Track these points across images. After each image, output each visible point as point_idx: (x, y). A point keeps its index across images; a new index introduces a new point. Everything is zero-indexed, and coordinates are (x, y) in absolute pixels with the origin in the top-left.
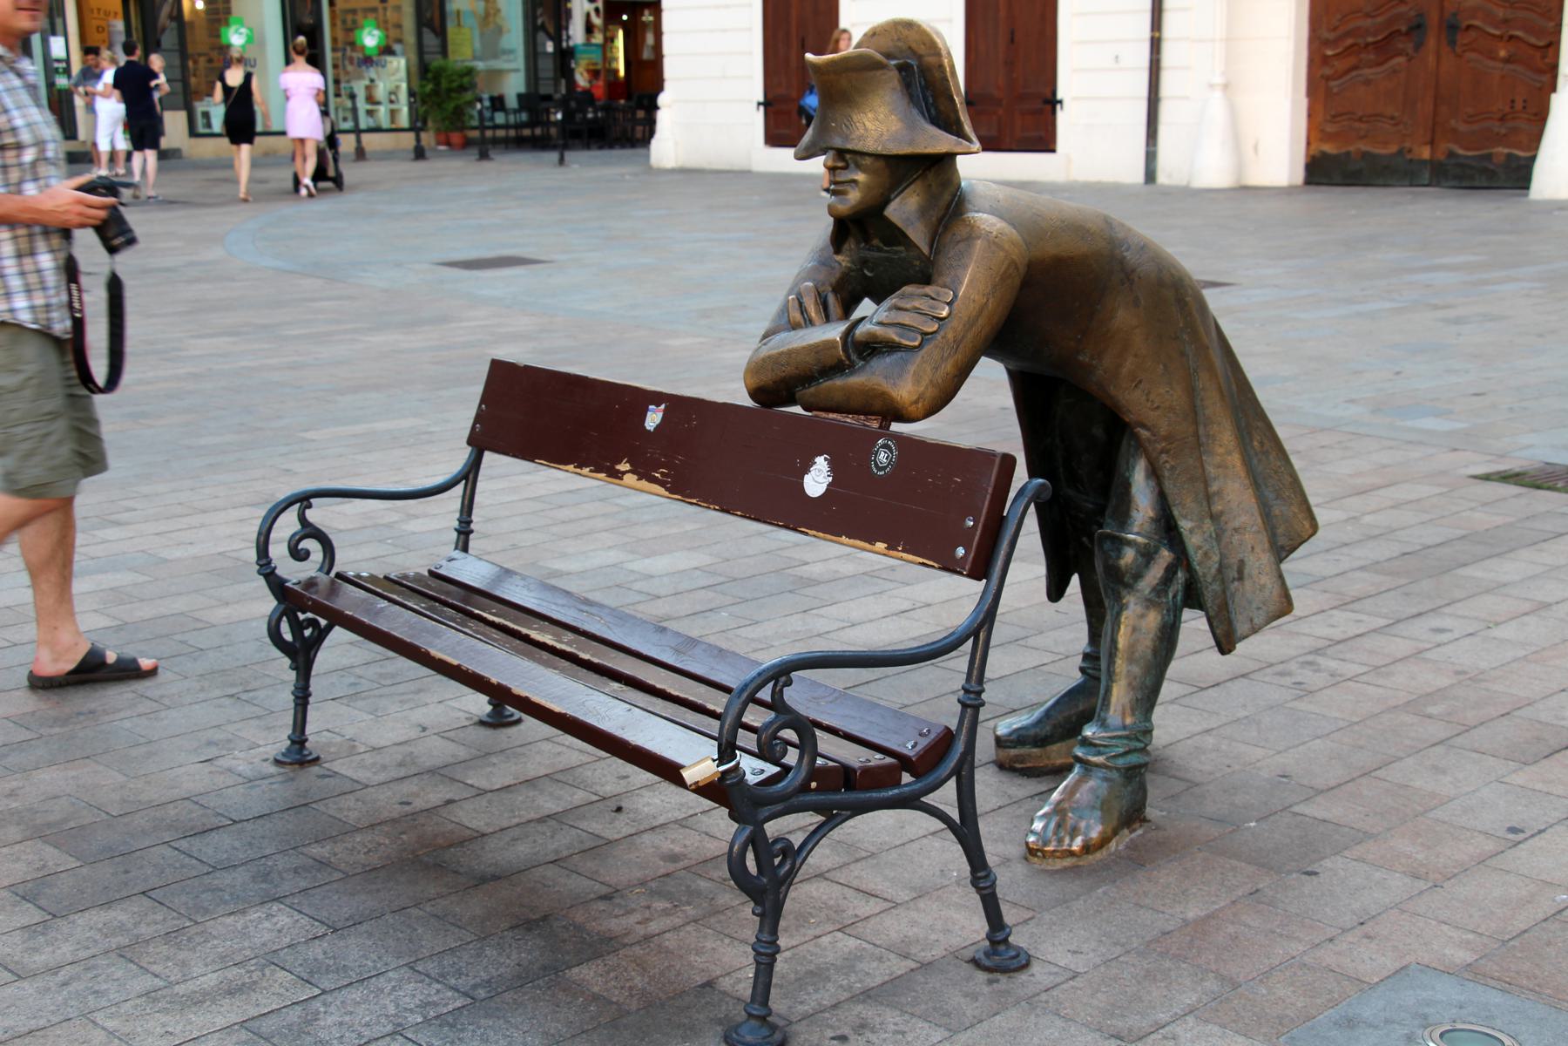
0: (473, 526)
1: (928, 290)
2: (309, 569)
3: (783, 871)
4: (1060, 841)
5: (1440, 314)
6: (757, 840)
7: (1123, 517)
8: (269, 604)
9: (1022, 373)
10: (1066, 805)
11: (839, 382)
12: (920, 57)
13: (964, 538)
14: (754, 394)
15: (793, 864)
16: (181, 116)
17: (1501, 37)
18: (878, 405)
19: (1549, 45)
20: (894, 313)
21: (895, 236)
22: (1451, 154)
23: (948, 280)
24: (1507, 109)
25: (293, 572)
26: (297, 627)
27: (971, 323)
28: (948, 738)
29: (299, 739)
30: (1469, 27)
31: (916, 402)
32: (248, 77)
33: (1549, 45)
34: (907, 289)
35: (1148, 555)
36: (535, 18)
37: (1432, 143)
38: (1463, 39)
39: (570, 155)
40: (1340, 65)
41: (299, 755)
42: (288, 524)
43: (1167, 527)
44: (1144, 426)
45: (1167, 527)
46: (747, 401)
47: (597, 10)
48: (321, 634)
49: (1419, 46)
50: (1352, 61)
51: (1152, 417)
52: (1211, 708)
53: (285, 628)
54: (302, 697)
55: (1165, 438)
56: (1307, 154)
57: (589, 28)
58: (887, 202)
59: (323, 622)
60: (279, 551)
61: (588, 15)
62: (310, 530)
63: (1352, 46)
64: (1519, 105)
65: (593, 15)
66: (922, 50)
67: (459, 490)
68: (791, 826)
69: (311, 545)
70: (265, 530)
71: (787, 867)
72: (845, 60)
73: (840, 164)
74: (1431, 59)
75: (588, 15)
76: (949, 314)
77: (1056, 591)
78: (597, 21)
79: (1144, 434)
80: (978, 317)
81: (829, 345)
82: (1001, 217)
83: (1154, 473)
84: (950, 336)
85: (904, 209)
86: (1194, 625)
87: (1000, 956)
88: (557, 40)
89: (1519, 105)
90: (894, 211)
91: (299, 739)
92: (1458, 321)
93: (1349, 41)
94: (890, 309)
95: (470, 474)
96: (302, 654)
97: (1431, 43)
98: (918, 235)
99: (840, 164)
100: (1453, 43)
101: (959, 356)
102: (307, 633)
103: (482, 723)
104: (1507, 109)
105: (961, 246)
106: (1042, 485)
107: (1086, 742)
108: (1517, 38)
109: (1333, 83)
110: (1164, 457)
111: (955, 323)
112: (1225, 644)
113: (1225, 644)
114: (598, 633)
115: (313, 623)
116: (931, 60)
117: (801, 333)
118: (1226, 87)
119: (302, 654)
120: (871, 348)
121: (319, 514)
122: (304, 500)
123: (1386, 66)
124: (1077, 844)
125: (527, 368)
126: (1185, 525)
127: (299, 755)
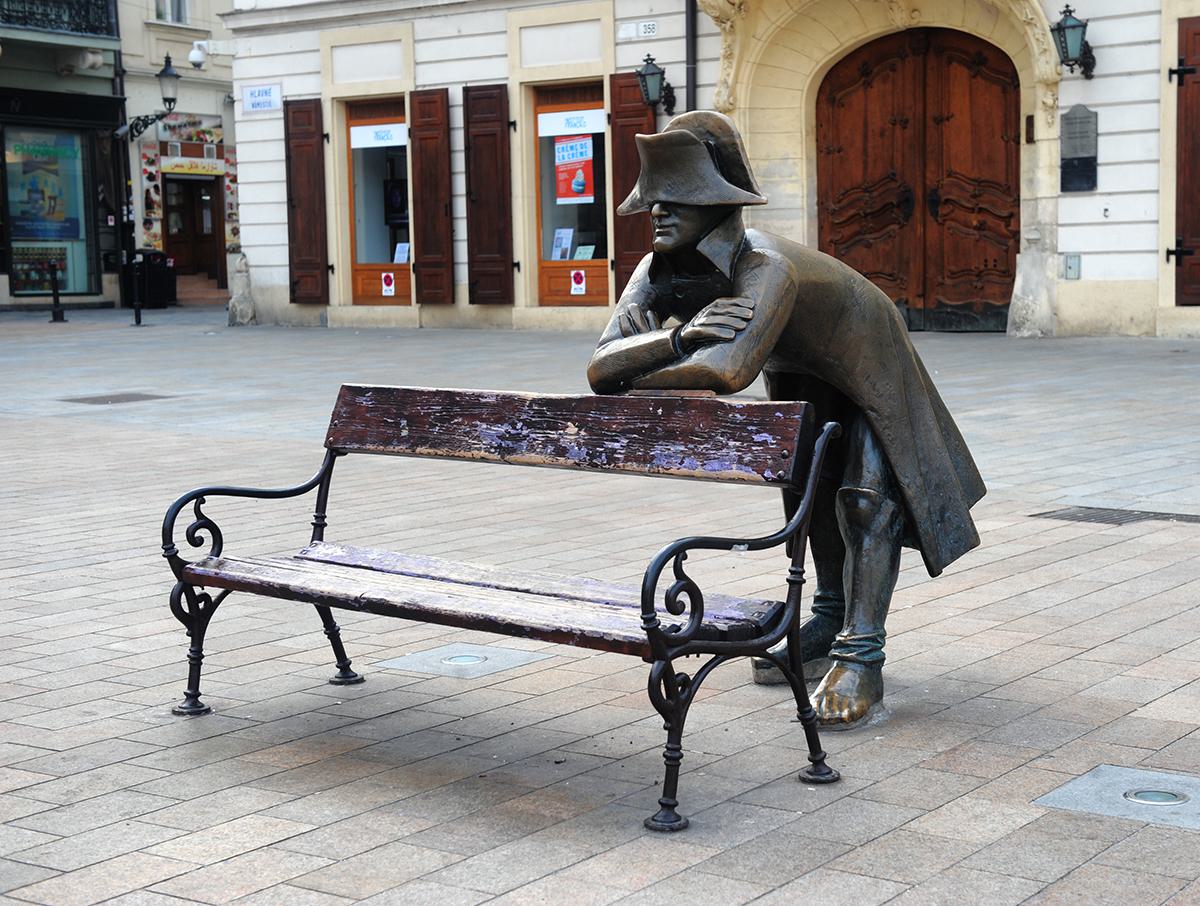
0: (326, 520)
1: (734, 301)
3: (683, 697)
4: (832, 711)
6: (666, 673)
7: (857, 476)
8: (172, 580)
10: (832, 689)
12: (717, 138)
14: (595, 386)
15: (690, 691)
17: (973, 209)
19: (1011, 215)
20: (712, 317)
21: (706, 265)
22: (941, 304)
24: (982, 267)
26: (193, 600)
27: (769, 321)
28: (782, 607)
29: (193, 694)
30: (947, 201)
31: (734, 378)
33: (1011, 215)
35: (876, 506)
36: (96, 194)
37: (923, 296)
38: (943, 210)
39: (147, 317)
40: (847, 231)
41: (194, 706)
42: (187, 517)
43: (891, 483)
44: (873, 409)
45: (891, 483)
46: (593, 394)
47: (156, 187)
48: (212, 606)
49: (908, 216)
50: (855, 227)
51: (877, 403)
52: (930, 619)
54: (196, 659)
55: (888, 418)
57: (149, 204)
58: (699, 240)
60: (179, 537)
61: (148, 191)
62: (204, 522)
63: (853, 216)
64: (991, 265)
65: (152, 191)
66: (718, 132)
68: (686, 665)
69: (204, 533)
70: (168, 524)
71: (686, 693)
72: (661, 139)
74: (920, 230)
75: (148, 191)
76: (753, 316)
78: (157, 198)
79: (873, 415)
80: (772, 318)
82: (780, 251)
83: (878, 443)
86: (910, 558)
87: (819, 773)
88: (119, 216)
89: (991, 265)
90: (703, 247)
91: (193, 694)
93: (852, 212)
95: (323, 481)
96: (196, 620)
97: (918, 213)
98: (724, 265)
100: (935, 214)
101: (761, 347)
102: (201, 605)
103: (332, 682)
104: (982, 267)
105: (756, 271)
106: (836, 426)
107: (841, 645)
108: (986, 209)
109: (841, 247)
110: (887, 431)
112: (934, 572)
113: (934, 572)
114: (429, 605)
116: (725, 139)
119: (196, 620)
120: (699, 341)
121: (212, 507)
122: (199, 496)
123: (885, 231)
124: (845, 713)
126: (904, 481)
127: (194, 706)
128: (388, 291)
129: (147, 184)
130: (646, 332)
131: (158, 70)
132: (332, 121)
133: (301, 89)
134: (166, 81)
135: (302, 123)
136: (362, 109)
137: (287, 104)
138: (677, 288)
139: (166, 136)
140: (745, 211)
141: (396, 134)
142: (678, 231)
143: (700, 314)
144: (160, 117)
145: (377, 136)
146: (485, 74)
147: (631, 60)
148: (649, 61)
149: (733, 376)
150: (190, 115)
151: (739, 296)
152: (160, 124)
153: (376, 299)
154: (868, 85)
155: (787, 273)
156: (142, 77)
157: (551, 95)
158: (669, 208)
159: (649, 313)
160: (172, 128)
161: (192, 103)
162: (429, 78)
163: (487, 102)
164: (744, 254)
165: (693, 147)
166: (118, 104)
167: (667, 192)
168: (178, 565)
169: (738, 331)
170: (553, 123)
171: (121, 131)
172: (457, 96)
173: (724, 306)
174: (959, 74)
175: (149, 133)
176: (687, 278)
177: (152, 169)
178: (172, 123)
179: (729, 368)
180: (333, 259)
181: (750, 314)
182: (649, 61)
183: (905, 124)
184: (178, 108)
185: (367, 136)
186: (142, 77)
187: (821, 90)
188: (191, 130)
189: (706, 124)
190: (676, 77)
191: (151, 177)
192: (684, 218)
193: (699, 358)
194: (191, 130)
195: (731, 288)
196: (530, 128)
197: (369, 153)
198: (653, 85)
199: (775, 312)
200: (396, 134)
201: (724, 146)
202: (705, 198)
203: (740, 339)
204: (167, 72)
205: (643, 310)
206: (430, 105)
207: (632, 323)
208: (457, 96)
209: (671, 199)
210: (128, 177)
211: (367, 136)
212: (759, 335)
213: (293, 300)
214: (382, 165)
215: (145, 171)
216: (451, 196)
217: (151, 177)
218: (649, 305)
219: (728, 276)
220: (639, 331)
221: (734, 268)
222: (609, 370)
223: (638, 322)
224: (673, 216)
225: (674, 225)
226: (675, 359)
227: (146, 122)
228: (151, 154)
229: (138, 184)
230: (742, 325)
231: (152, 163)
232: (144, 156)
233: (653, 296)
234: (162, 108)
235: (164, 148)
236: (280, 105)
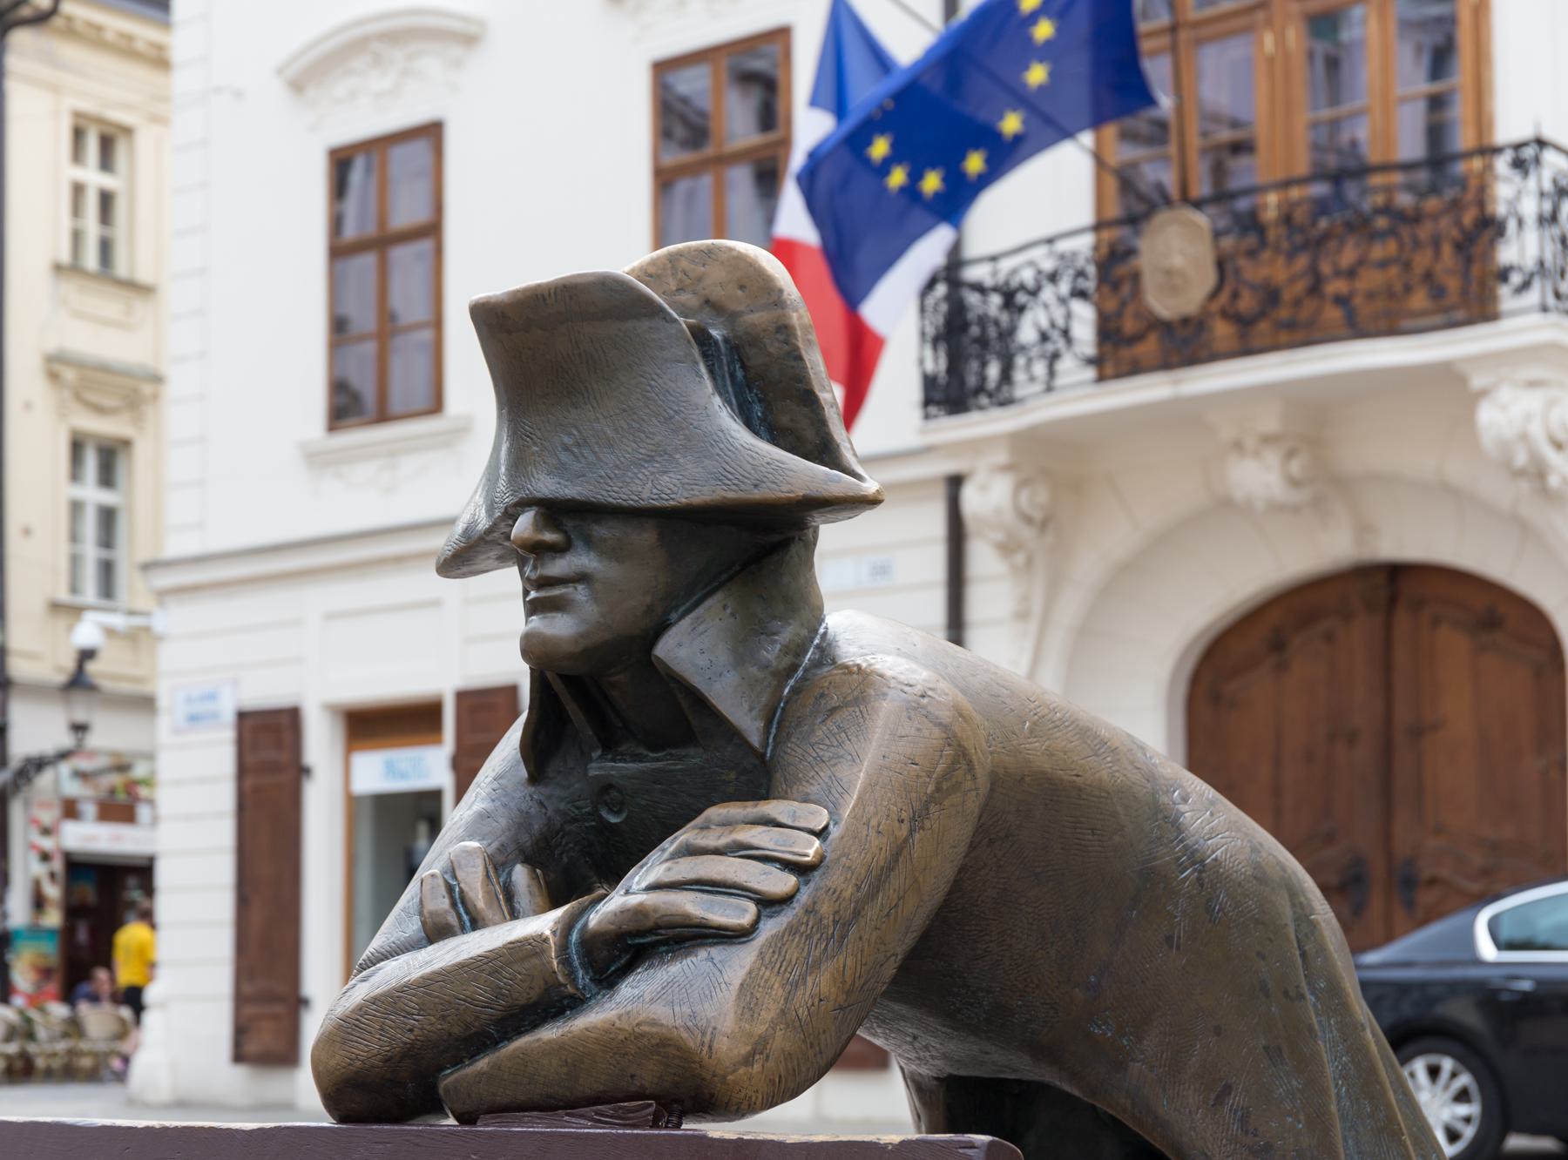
1: (773, 808)
9: (951, 1077)
11: (550, 1033)
13: (1045, 52)
18: (648, 1075)
21: (683, 716)
23: (814, 790)
27: (877, 881)
30: (1433, 882)
31: (748, 1060)
34: (714, 812)
46: (327, 1122)
47: (52, 876)
57: (39, 902)
58: (662, 627)
66: (736, 300)
73: (550, 537)
81: (529, 949)
84: (825, 909)
85: (695, 648)
94: (676, 855)
99: (550, 537)
101: (847, 960)
111: (833, 879)
116: (758, 318)
117: (451, 943)
129: (38, 869)
130: (495, 924)
131: (61, 678)
132: (320, 743)
133: (265, 693)
134: (79, 697)
135: (268, 748)
136: (370, 725)
137: (243, 717)
138: (605, 791)
139: (72, 788)
140: (831, 535)
142: (595, 598)
143: (654, 855)
144: (64, 755)
145: (390, 770)
149: (744, 1050)
150: (115, 754)
151: (784, 797)
152: (65, 769)
154: (1282, 668)
155: (945, 727)
156: (38, 691)
158: (569, 524)
159: (520, 874)
160: (82, 776)
161: (111, 734)
164: (812, 689)
165: (645, 324)
167: (560, 470)
169: (768, 904)
173: (728, 824)
174: (1453, 645)
176: (637, 758)
177: (47, 843)
178: (83, 764)
179: (728, 1023)
181: (810, 849)
183: (1352, 738)
184: (94, 740)
185: (379, 771)
186: (38, 691)
187: (1196, 680)
188: (116, 779)
189: (700, 279)
191: (45, 857)
192: (613, 553)
193: (644, 998)
194: (116, 779)
195: (758, 777)
199: (899, 851)
201: (754, 340)
202: (678, 484)
203: (771, 928)
204: (78, 682)
205: (498, 865)
207: (458, 898)
209: (570, 491)
211: (379, 771)
212: (844, 924)
213: (239, 1057)
215: (33, 847)
217: (45, 857)
218: (522, 850)
219: (755, 740)
220: (476, 923)
221: (779, 718)
222: (370, 1049)
223: (478, 896)
224: (578, 543)
225: (582, 578)
226: (557, 1003)
227: (38, 764)
230: (778, 882)
231: (46, 831)
232: (34, 821)
233: (537, 826)
234: (66, 740)
235: (70, 810)
236: (229, 717)
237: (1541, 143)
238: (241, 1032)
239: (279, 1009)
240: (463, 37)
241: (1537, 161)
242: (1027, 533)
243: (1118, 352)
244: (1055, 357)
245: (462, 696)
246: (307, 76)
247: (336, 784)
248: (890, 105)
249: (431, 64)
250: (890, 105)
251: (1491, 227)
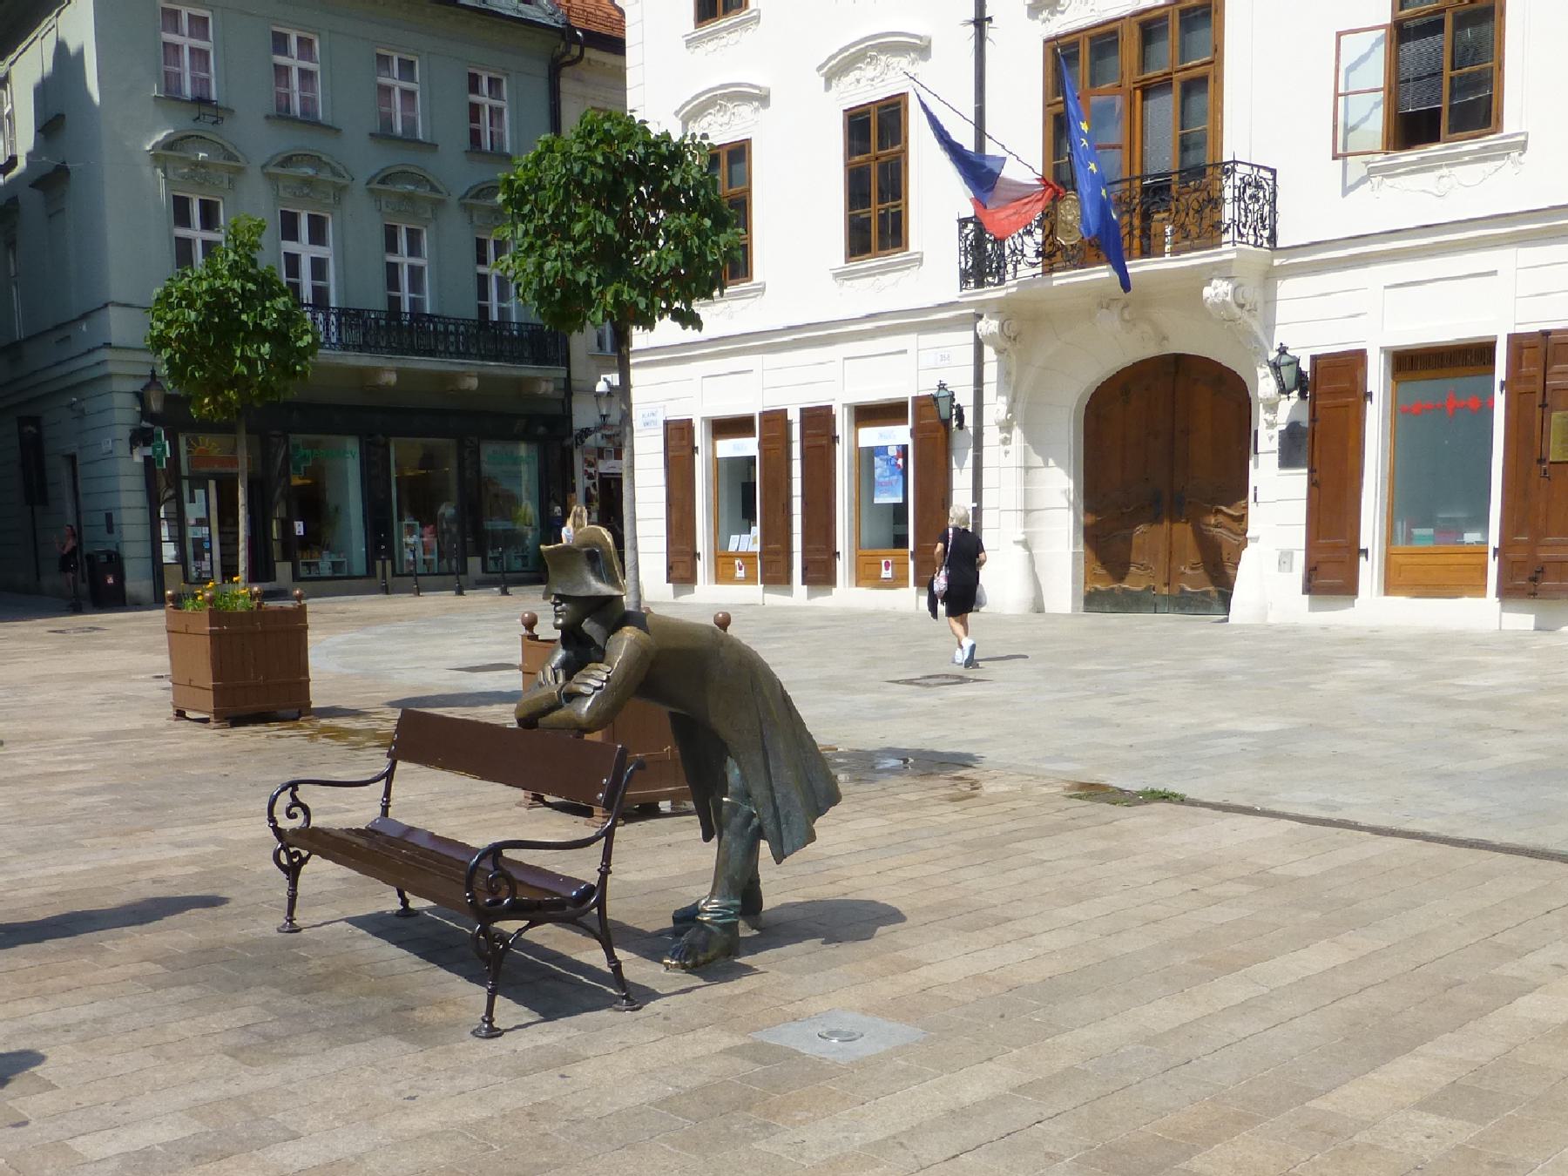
2: (298, 822)
5: (1126, 698)
13: (601, 788)
14: (520, 721)
16: (288, 566)
22: (1182, 590)
25: (285, 824)
26: (290, 856)
32: (666, 815)
42: (284, 800)
48: (304, 861)
53: (283, 855)
56: (373, 823)
59: (304, 853)
62: (296, 802)
67: (383, 783)
77: (748, 970)
92: (1125, 703)
95: (389, 776)
96: (292, 872)
115: (297, 853)
118: (1026, 544)
119: (292, 872)
121: (304, 793)
122: (294, 785)
125: (486, 724)
128: (740, 574)
129: (589, 483)
132: (700, 437)
135: (678, 435)
136: (726, 427)
137: (666, 423)
139: (603, 443)
141: (748, 446)
146: (815, 398)
147: (928, 387)
148: (942, 386)
152: (599, 435)
153: (732, 580)
157: (867, 414)
162: (772, 403)
163: (818, 420)
166: (568, 417)
168: (278, 832)
170: (871, 436)
171: (568, 442)
172: (794, 416)
175: (590, 441)
177: (592, 470)
180: (699, 549)
182: (942, 386)
185: (731, 448)
190: (965, 398)
191: (590, 477)
196: (848, 440)
197: (733, 462)
198: (944, 407)
200: (748, 446)
206: (775, 421)
208: (794, 416)
210: (573, 477)
211: (731, 448)
214: (737, 474)
216: (789, 497)
217: (590, 477)
226: (558, 706)
227: (586, 432)
228: (591, 458)
229: (581, 482)
231: (591, 465)
235: (600, 453)
237: (1235, 162)
238: (670, 568)
239: (687, 558)
240: (763, 99)
241: (1234, 171)
242: (1008, 345)
243: (1051, 256)
244: (1018, 262)
245: (763, 415)
246: (838, 69)
247: (709, 453)
248: (1092, 519)
249: (745, 110)
250: (1092, 519)
251: (1216, 202)
